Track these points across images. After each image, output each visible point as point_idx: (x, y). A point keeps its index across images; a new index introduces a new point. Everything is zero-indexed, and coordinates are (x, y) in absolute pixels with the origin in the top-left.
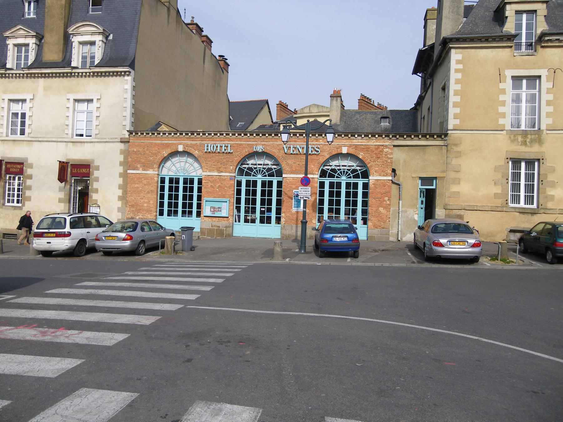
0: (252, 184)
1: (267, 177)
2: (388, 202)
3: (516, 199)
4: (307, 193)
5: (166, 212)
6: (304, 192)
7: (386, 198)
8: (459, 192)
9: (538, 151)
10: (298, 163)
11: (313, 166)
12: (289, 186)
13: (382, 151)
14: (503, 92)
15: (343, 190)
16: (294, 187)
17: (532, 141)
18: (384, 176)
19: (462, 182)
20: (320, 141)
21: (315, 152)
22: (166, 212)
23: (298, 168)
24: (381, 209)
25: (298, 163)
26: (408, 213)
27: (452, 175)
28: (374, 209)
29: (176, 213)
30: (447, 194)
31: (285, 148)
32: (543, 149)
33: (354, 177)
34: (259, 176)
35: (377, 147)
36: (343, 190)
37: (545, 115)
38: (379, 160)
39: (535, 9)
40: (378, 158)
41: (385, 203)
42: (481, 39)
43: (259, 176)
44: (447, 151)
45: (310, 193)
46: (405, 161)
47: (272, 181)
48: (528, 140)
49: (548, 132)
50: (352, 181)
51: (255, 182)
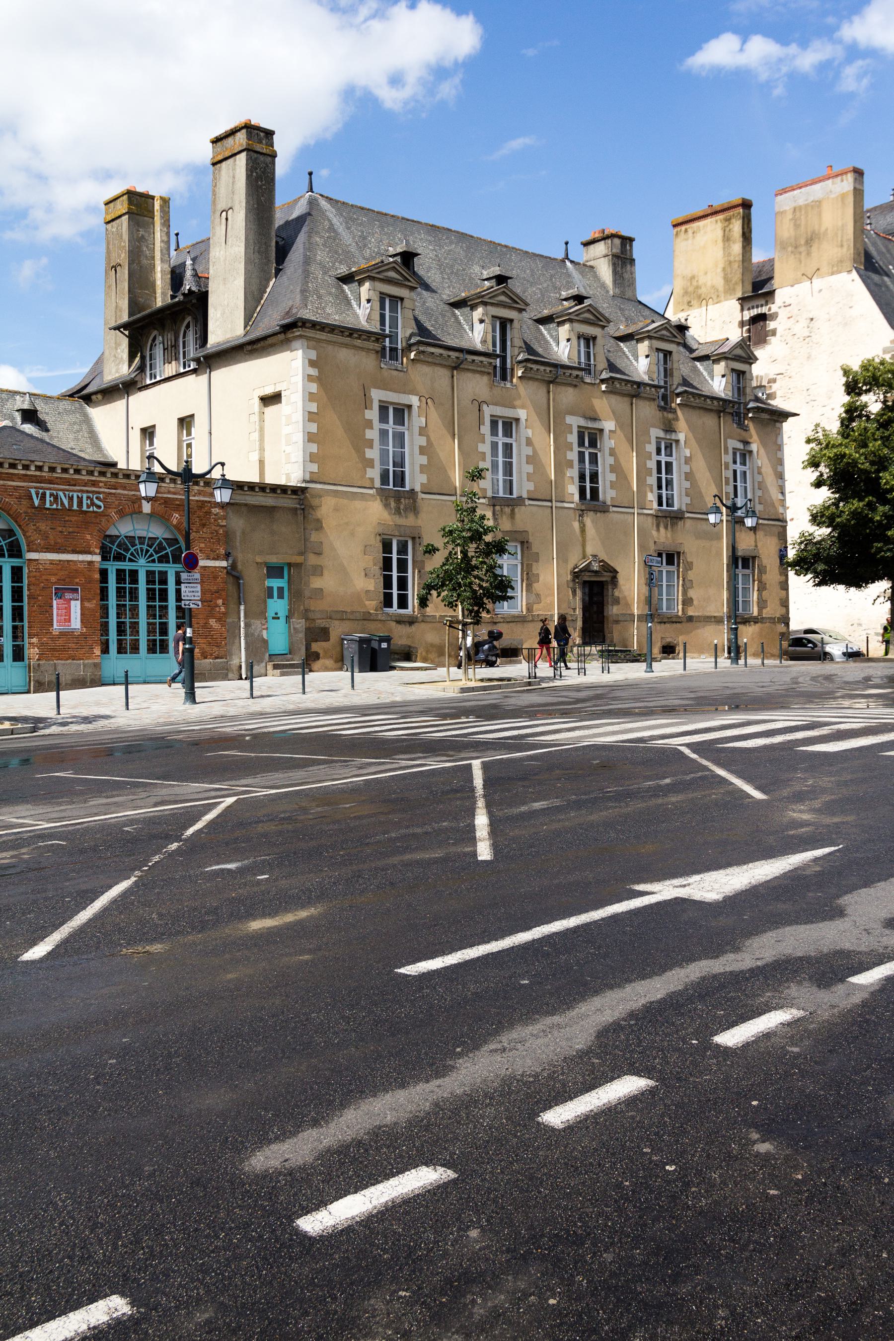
0: (128, 578)
1: (157, 564)
2: (223, 609)
3: (388, 602)
4: (196, 594)
5: (113, 647)
6: (190, 594)
7: (220, 602)
8: (322, 590)
9: (413, 524)
10: (60, 529)
11: (88, 537)
12: (44, 577)
13: (209, 513)
14: (369, 424)
15: (142, 586)
16: (53, 579)
17: (406, 510)
18: (214, 559)
19: (325, 572)
20: (101, 484)
21: (95, 509)
22: (113, 647)
23: (59, 541)
24: (212, 622)
25: (60, 529)
26: (253, 627)
27: (312, 560)
28: (202, 622)
29: (135, 649)
30: (307, 593)
31: (34, 496)
32: (419, 522)
33: (160, 560)
34: (142, 561)
35: (200, 504)
36: (142, 586)
37: (419, 469)
38: (204, 530)
39: (402, 296)
40: (204, 525)
41: (217, 609)
42: (342, 332)
43: (142, 561)
44: (304, 517)
45: (199, 594)
46: (243, 533)
47: (166, 572)
48: (402, 507)
49: (424, 496)
50: (158, 567)
51: (134, 574)
